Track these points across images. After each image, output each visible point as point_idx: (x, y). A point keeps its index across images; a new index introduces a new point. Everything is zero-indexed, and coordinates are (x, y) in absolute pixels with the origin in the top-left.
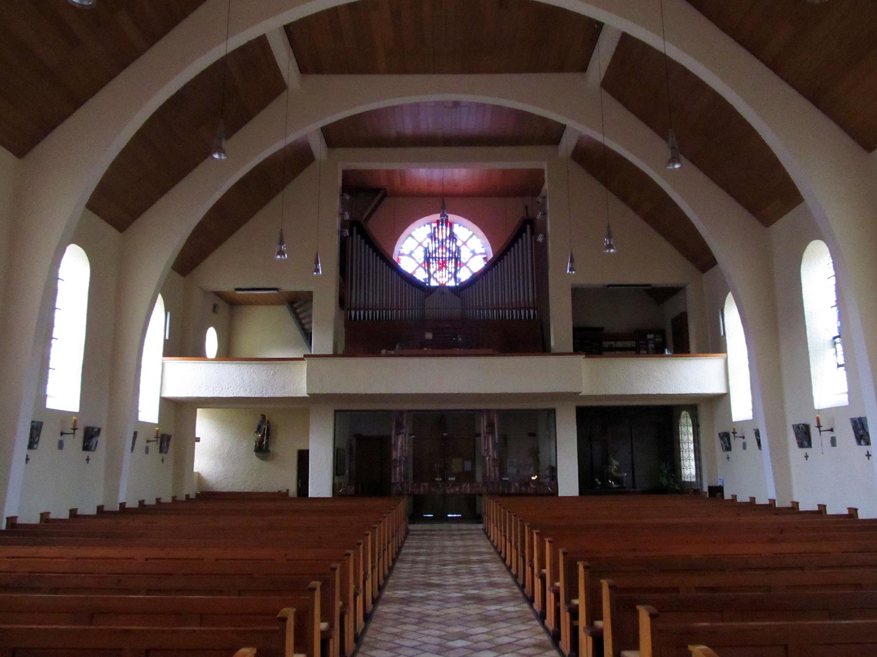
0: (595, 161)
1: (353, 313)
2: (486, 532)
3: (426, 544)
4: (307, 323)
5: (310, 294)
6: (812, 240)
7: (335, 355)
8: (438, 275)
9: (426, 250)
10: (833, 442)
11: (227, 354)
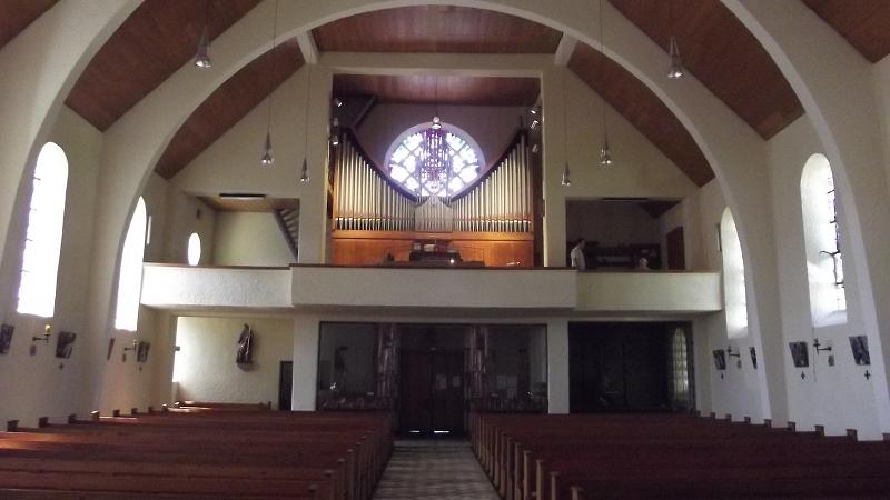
0: (592, 69)
2: (474, 450)
3: (411, 463)
5: (297, 201)
8: (429, 185)
9: (418, 158)
10: (831, 361)
11: (210, 260)
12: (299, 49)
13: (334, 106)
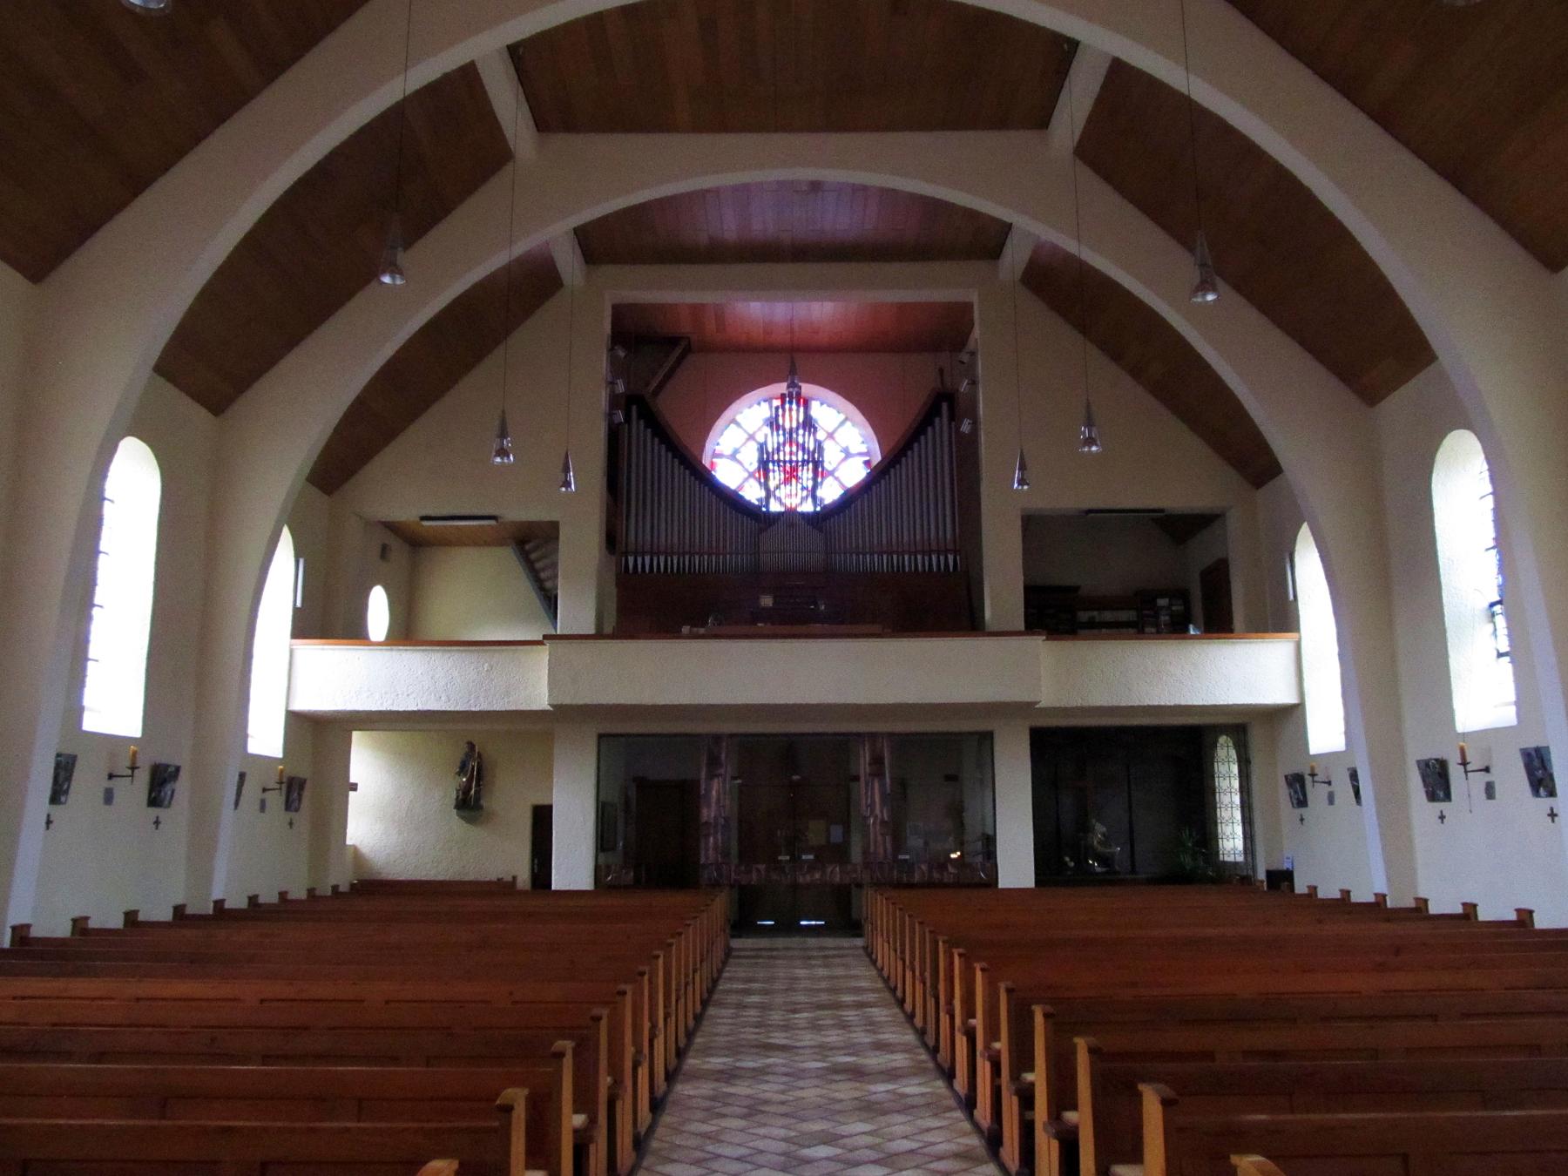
0: (1064, 288)
1: (631, 560)
2: (869, 952)
3: (761, 974)
4: (549, 579)
5: (554, 526)
6: (1451, 430)
7: (599, 635)
8: (783, 492)
9: (762, 448)
10: (1490, 791)
11: (405, 633)
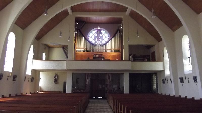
0: (134, 16)
2: (107, 102)
3: (93, 105)
5: (67, 46)
8: (97, 42)
9: (95, 36)
10: (189, 82)
11: (48, 59)
12: (68, 11)
13: (76, 24)
